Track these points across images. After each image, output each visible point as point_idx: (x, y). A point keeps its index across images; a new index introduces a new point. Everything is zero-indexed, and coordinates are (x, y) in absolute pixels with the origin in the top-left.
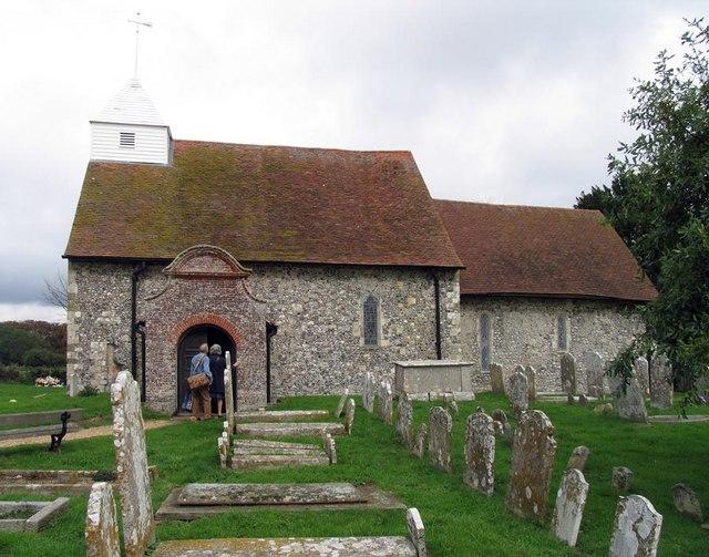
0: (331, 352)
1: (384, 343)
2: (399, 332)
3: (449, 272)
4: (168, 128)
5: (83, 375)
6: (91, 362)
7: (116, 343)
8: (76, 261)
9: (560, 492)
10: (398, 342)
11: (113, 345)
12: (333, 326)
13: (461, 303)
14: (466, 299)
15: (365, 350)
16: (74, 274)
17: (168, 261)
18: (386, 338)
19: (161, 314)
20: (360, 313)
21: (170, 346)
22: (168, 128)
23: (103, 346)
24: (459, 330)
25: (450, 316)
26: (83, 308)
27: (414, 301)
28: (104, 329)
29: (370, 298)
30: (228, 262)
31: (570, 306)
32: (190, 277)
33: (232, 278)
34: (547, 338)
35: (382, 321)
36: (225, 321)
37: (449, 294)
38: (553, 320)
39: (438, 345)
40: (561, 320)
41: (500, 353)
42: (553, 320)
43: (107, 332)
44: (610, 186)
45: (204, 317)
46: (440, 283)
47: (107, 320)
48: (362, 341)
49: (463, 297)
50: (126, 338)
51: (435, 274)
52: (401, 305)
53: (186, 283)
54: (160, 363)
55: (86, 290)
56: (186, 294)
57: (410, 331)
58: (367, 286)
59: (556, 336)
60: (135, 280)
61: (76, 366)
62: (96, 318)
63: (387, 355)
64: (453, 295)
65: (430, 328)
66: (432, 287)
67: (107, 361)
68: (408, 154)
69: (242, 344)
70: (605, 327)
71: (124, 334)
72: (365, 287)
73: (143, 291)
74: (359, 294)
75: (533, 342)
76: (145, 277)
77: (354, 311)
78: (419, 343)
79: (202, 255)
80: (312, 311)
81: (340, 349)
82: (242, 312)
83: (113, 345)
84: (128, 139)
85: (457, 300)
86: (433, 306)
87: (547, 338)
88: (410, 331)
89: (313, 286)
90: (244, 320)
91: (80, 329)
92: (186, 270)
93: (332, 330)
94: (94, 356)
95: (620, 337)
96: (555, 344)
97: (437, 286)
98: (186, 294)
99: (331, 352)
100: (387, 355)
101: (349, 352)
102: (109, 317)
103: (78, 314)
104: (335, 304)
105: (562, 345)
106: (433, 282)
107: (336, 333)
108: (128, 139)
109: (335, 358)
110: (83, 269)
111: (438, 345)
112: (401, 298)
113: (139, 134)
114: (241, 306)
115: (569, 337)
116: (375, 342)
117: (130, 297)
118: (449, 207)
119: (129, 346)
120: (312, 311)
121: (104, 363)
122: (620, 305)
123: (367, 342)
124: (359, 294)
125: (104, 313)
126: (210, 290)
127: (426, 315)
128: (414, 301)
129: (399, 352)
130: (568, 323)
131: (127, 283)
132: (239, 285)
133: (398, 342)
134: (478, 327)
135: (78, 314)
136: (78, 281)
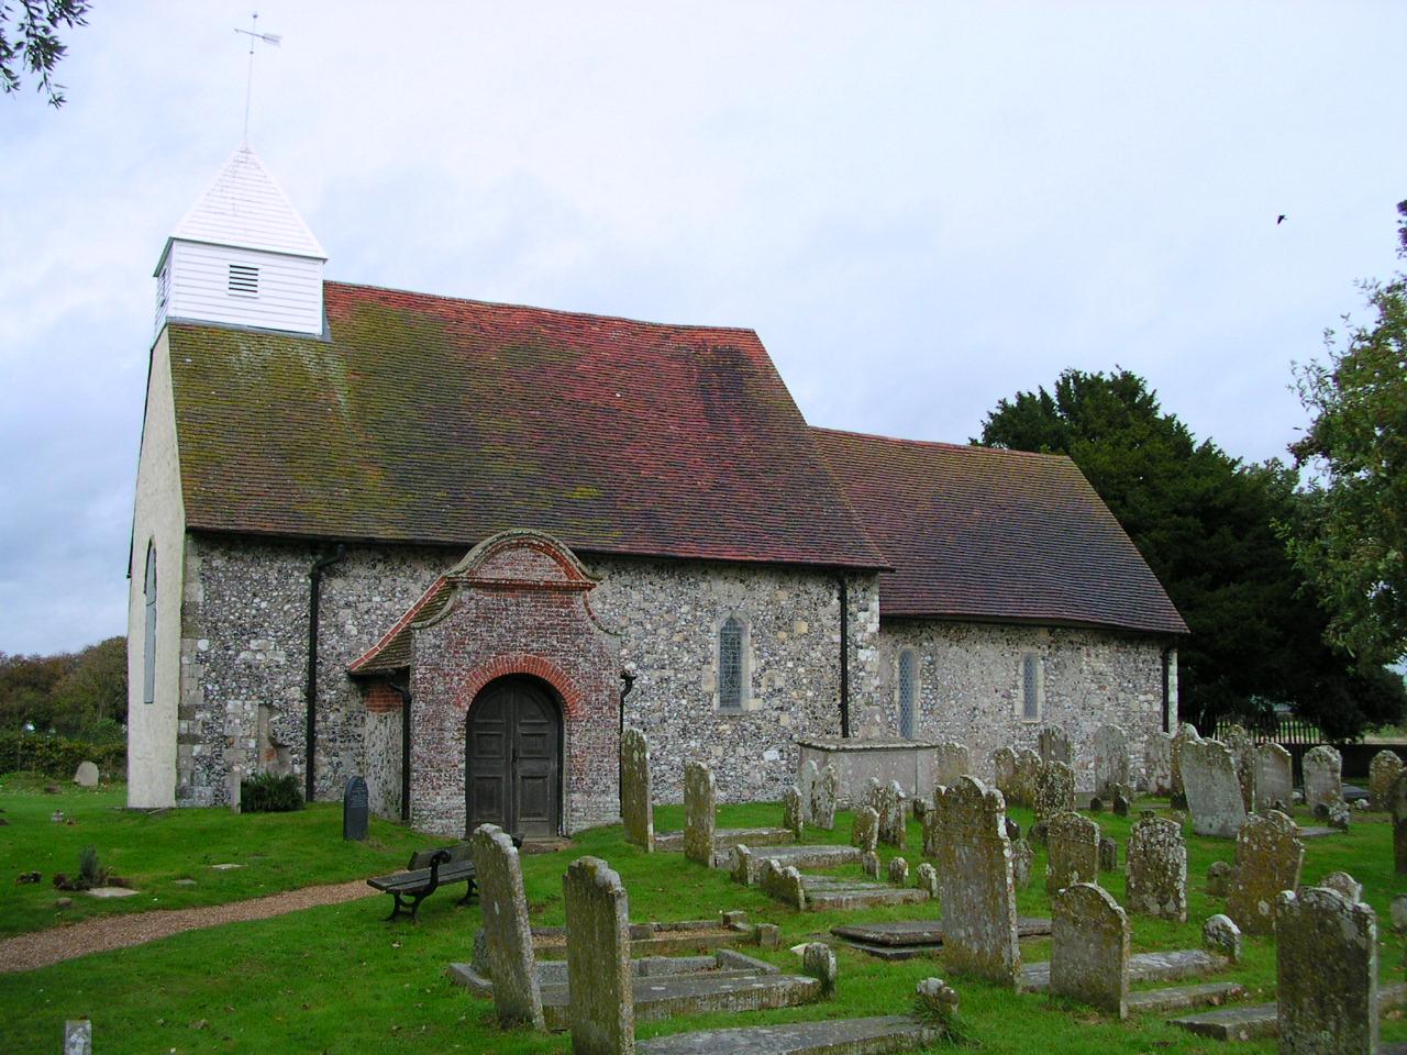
0: (663, 720)
1: (752, 704)
2: (779, 683)
3: (867, 574)
4: (172, 240)
5: (210, 767)
6: (225, 741)
7: (276, 703)
8: (202, 538)
9: (976, 952)
10: (776, 702)
11: (270, 706)
12: (668, 673)
13: (880, 631)
14: (889, 622)
15: (722, 717)
16: (196, 563)
17: (459, 550)
18: (757, 696)
19: (441, 656)
20: (715, 648)
21: (456, 715)
22: (172, 240)
23: (251, 708)
24: (876, 682)
25: (863, 655)
26: (213, 632)
27: (804, 627)
28: (254, 675)
29: (731, 621)
30: (560, 560)
31: (1043, 635)
32: (496, 587)
33: (568, 589)
34: (1008, 696)
35: (750, 664)
36: (552, 667)
37: (862, 615)
38: (1017, 664)
39: (843, 707)
40: (1029, 663)
41: (930, 722)
42: (1017, 664)
43: (259, 680)
44: (1052, 393)
45: (517, 660)
46: (850, 593)
47: (259, 656)
48: (716, 701)
49: (883, 618)
50: (296, 693)
51: (840, 576)
52: (782, 635)
53: (488, 598)
54: (438, 745)
55: (221, 596)
56: (486, 617)
57: (796, 684)
58: (723, 592)
59: (1021, 693)
60: (316, 578)
61: (197, 748)
62: (237, 655)
63: (758, 728)
64: (868, 620)
65: (831, 677)
66: (835, 602)
67: (258, 738)
68: (750, 335)
69: (581, 710)
70: (1098, 676)
71: (292, 684)
72: (724, 600)
73: (330, 600)
74: (714, 614)
75: (985, 703)
76: (333, 574)
77: (704, 645)
78: (810, 706)
79: (518, 546)
80: (633, 643)
81: (680, 715)
82: (583, 652)
83: (270, 706)
84: (243, 280)
85: (874, 627)
86: (837, 638)
87: (1008, 696)
88: (796, 684)
89: (636, 596)
90: (585, 666)
91: (207, 674)
92: (488, 574)
93: (667, 680)
94: (235, 729)
95: (1122, 695)
96: (1019, 707)
97: (843, 599)
98: (486, 617)
99: (663, 720)
100: (758, 728)
101: (693, 721)
102: (264, 652)
103: (203, 644)
104: (673, 631)
105: (1030, 709)
106: (836, 594)
107: (673, 686)
108: (243, 280)
109: (671, 731)
110: (216, 554)
111: (843, 707)
112: (783, 622)
113: (268, 269)
114: (581, 641)
115: (1041, 696)
116: (737, 703)
117: (306, 611)
118: (815, 430)
119: (301, 710)
120: (633, 643)
121: (252, 744)
122: (1125, 636)
123: (723, 703)
124: (714, 614)
125: (253, 644)
126: (528, 611)
127: (823, 654)
128: (804, 627)
129: (778, 720)
130: (1040, 667)
131: (301, 582)
132: (578, 601)
133: (776, 702)
134: (897, 675)
135: (203, 644)
136: (205, 579)
